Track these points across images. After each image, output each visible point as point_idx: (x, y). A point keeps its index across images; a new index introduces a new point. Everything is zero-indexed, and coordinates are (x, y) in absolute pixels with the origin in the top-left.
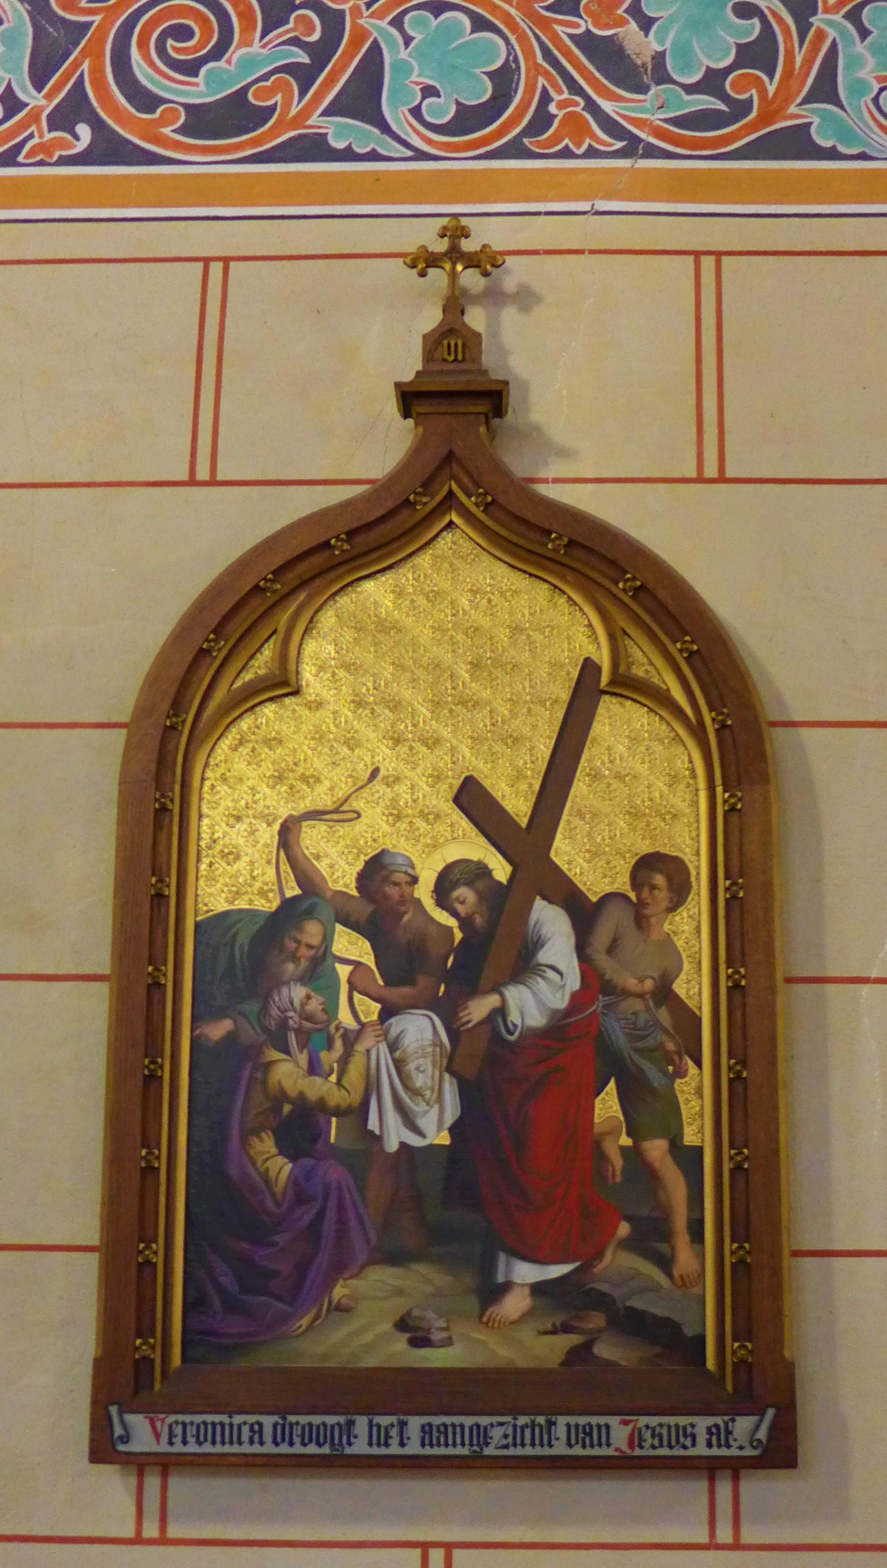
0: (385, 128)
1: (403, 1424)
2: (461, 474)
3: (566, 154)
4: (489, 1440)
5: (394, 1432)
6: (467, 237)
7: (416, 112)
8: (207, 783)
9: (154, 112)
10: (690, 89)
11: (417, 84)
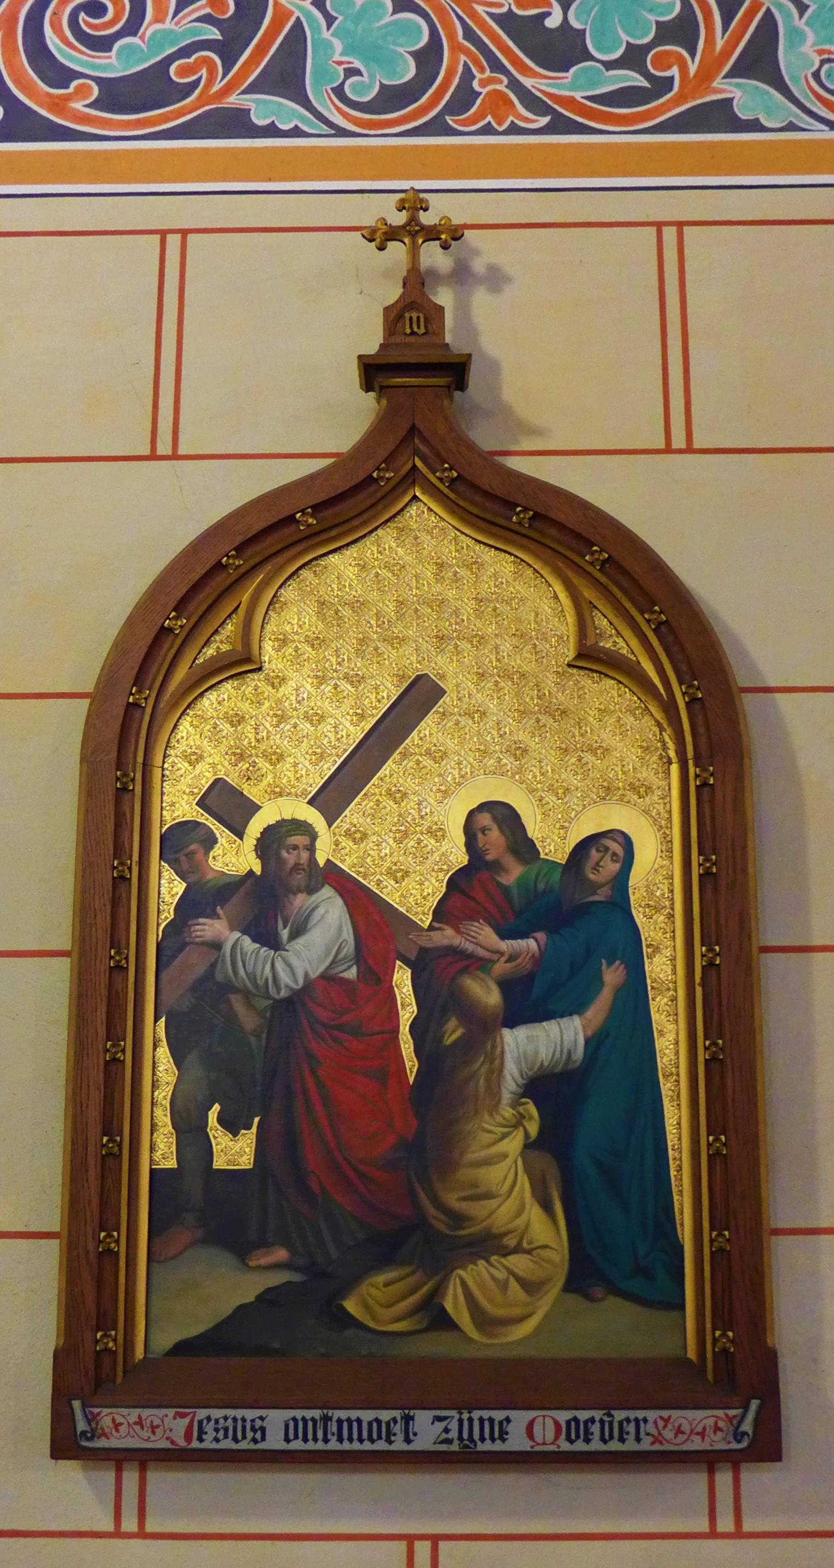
0: (307, 105)
1: (408, 1419)
2: (422, 447)
3: (488, 130)
4: (393, 1438)
5: (398, 1428)
6: (426, 210)
7: (339, 91)
8: (170, 760)
9: (67, 87)
10: (609, 65)
11: (340, 63)
